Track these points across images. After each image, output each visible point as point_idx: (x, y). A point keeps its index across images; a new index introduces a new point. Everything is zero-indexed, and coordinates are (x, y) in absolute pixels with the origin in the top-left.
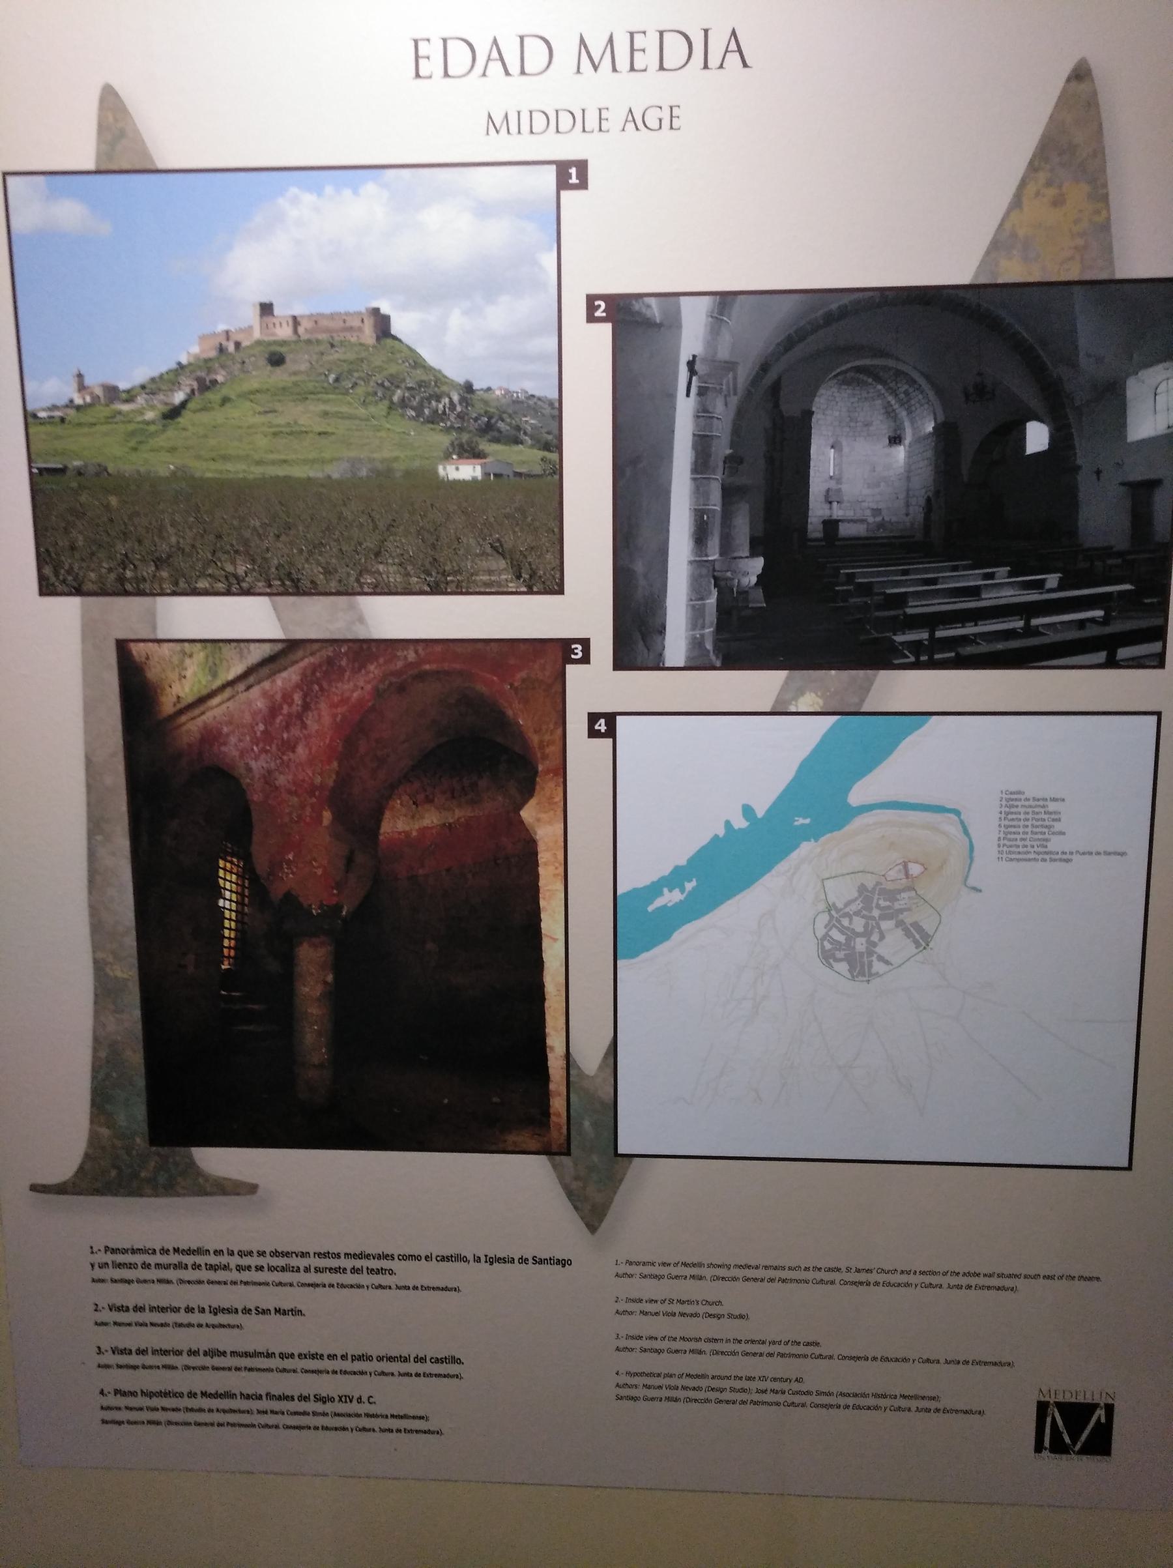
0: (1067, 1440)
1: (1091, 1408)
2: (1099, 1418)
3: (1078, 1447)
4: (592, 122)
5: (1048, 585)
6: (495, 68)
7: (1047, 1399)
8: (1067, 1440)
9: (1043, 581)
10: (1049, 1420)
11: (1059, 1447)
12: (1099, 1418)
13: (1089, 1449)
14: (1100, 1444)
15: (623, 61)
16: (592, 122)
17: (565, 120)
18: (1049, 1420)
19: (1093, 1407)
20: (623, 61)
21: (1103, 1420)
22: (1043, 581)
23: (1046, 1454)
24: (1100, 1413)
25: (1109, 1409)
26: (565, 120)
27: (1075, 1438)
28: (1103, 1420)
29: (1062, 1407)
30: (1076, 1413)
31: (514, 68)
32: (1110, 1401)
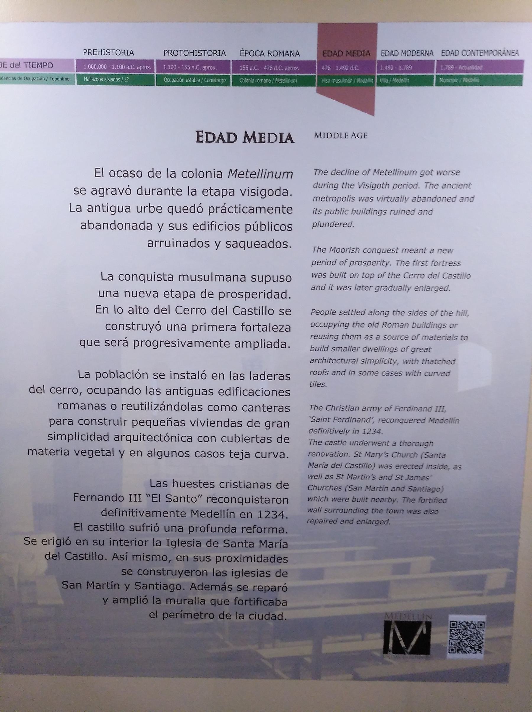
0: (403, 644)
1: (417, 624)
2: (422, 631)
3: (409, 650)
4: (343, 136)
5: (490, 585)
6: (221, 141)
7: (390, 620)
8: (403, 644)
9: (483, 578)
10: (391, 634)
11: (398, 650)
12: (422, 631)
13: (416, 651)
14: (423, 648)
15: (258, 139)
16: (343, 136)
17: (336, 135)
18: (391, 634)
19: (419, 624)
20: (258, 139)
21: (425, 632)
22: (483, 578)
23: (390, 654)
24: (422, 629)
25: (429, 625)
26: (336, 135)
27: (407, 644)
28: (425, 632)
29: (400, 624)
30: (408, 628)
31: (226, 140)
32: (429, 620)
